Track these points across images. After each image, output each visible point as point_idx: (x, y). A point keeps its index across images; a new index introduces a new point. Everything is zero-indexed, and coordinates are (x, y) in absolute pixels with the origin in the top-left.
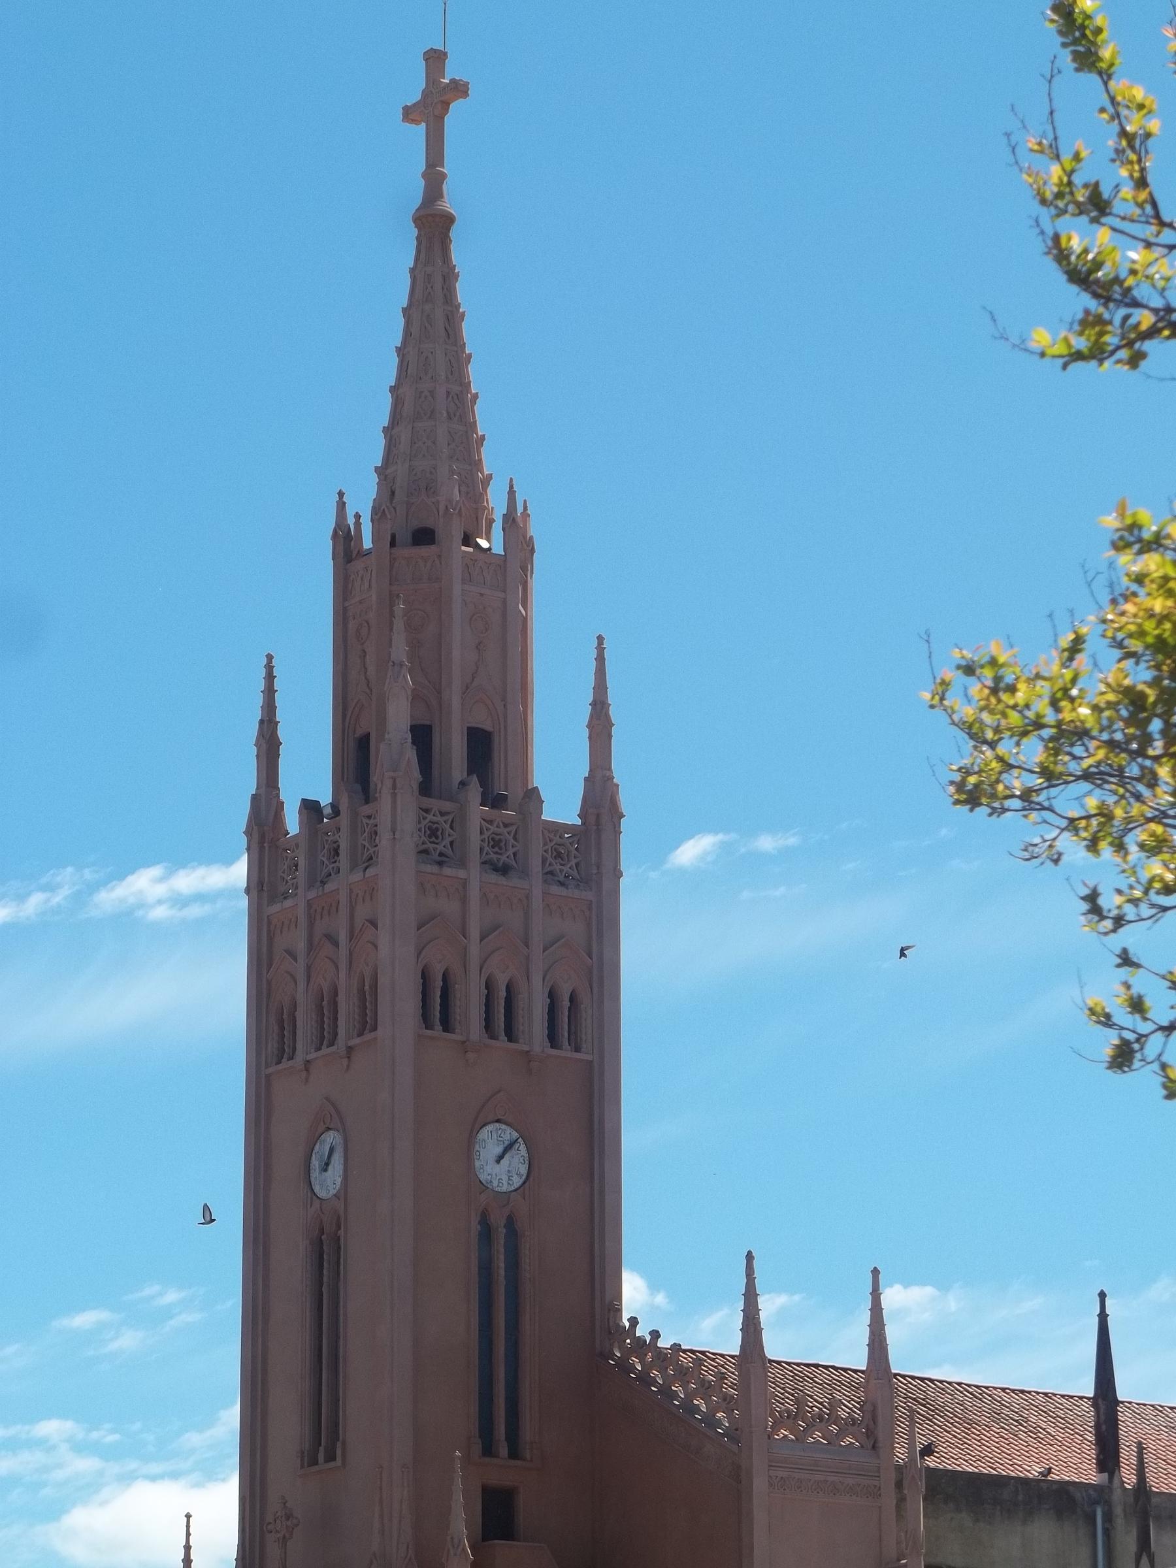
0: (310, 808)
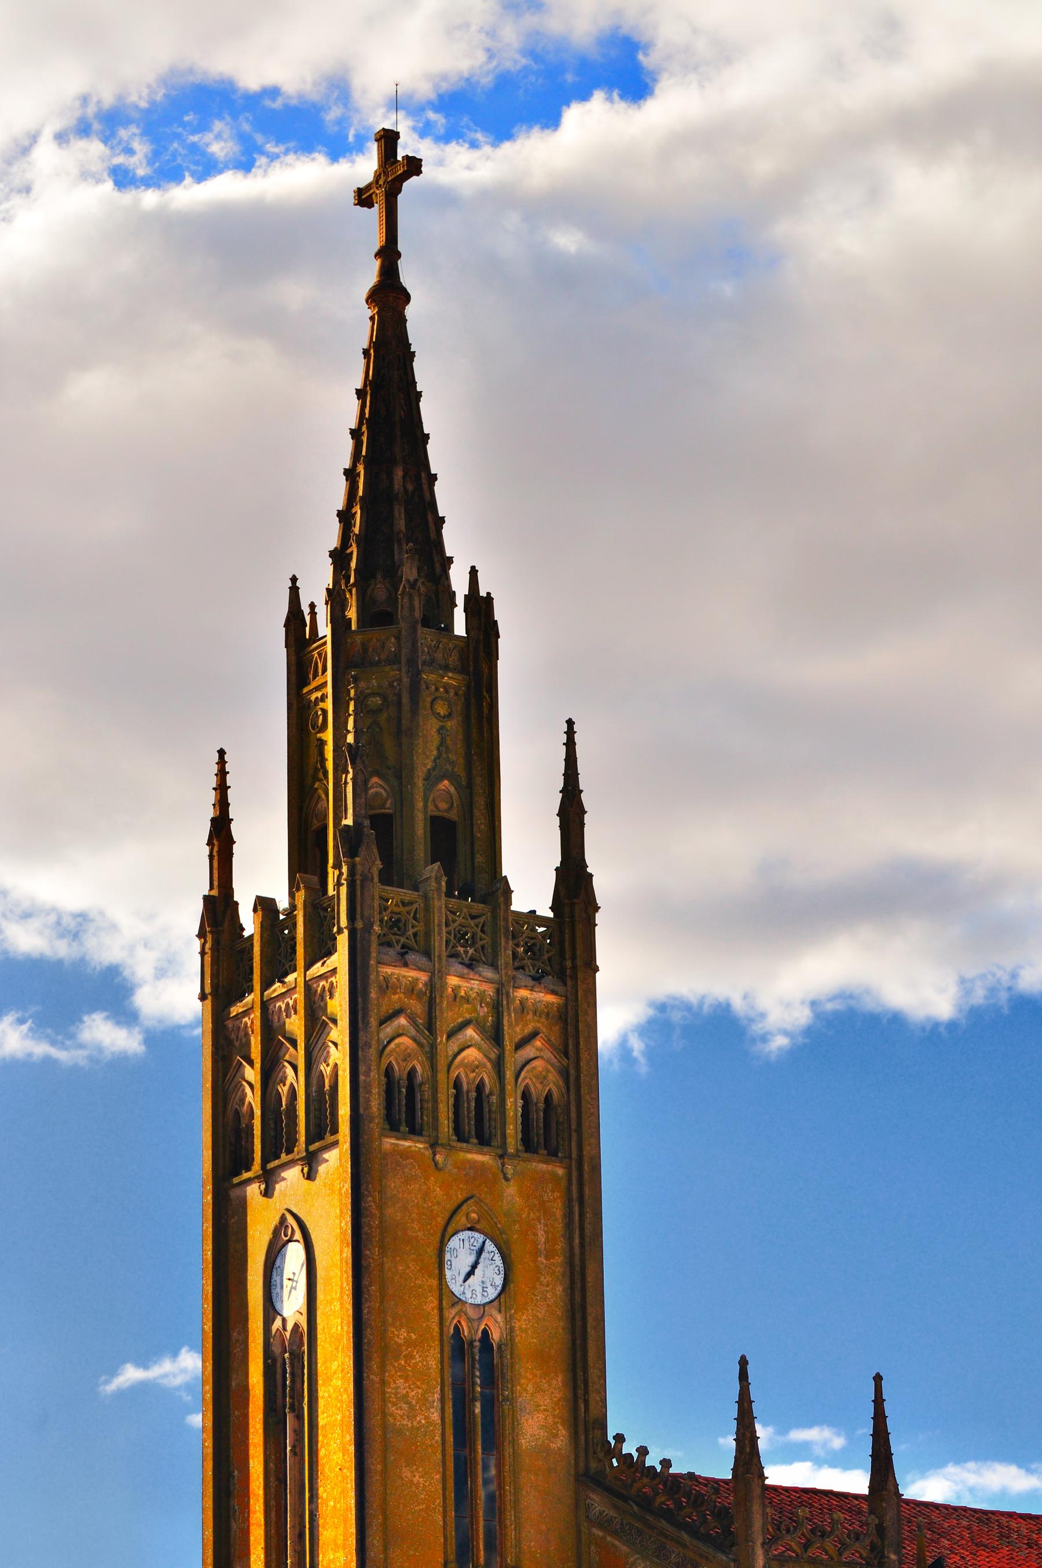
0: (264, 905)
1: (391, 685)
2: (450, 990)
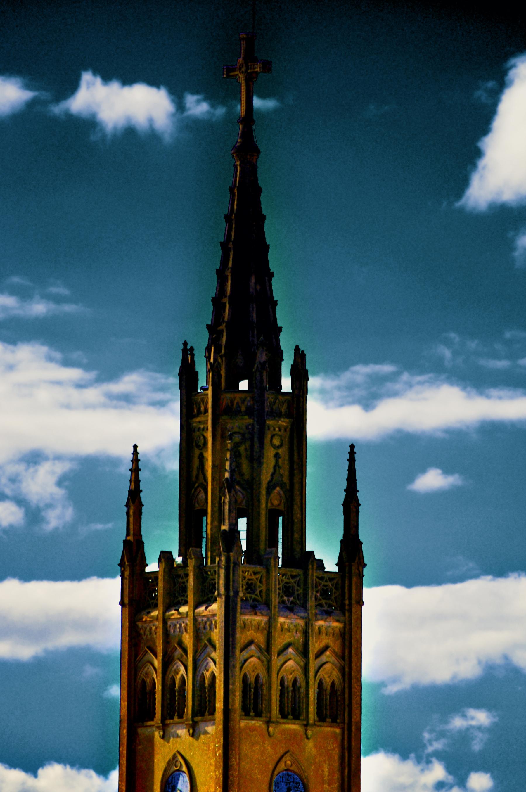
1: (247, 428)
2: (279, 625)
